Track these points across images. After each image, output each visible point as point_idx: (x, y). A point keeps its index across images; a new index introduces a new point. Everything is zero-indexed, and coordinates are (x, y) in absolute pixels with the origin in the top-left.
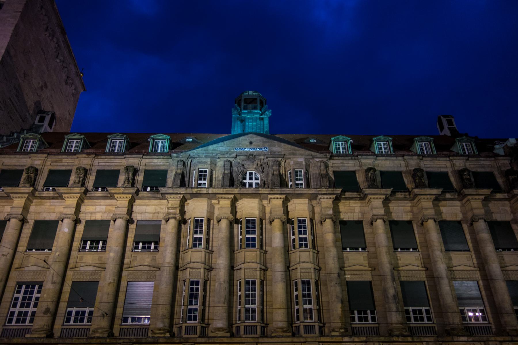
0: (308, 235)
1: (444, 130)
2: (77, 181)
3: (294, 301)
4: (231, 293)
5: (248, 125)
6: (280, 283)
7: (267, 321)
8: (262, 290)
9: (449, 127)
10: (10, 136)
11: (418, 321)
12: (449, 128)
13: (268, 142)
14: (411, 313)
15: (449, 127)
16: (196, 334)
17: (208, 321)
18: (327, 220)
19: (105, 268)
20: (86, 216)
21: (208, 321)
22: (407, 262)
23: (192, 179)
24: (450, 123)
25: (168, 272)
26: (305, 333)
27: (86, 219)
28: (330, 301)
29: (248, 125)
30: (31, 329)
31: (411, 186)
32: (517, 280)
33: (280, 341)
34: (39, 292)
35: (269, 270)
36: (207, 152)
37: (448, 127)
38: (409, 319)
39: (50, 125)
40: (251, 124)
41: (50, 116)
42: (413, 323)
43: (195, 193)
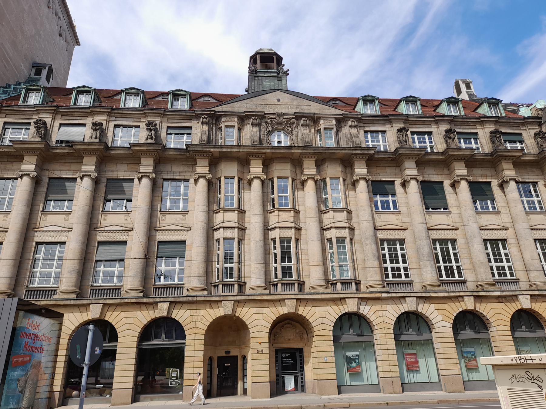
0: (341, 193)
1: (461, 94)
2: (94, 136)
3: (329, 259)
4: (266, 252)
5: (266, 84)
6: (317, 241)
7: (303, 279)
8: (297, 248)
9: (468, 91)
10: (6, 88)
11: (502, 277)
12: (467, 92)
13: (296, 100)
14: (389, 270)
15: (468, 91)
16: (234, 292)
17: (244, 279)
18: (86, 179)
19: (72, 229)
20: (174, 175)
21: (244, 279)
22: (439, 222)
23: (218, 137)
24: (468, 87)
25: (202, 231)
26: (342, 289)
27: (50, 177)
28: (366, 259)
29: (266, 84)
30: (121, 289)
31: (442, 146)
32: (545, 237)
33: (64, 301)
34: (402, 249)
35: (303, 229)
36: (233, 108)
37: (466, 92)
38: (387, 276)
39: (48, 79)
40: (269, 83)
41: (47, 68)
42: (391, 280)
43: (430, 153)
